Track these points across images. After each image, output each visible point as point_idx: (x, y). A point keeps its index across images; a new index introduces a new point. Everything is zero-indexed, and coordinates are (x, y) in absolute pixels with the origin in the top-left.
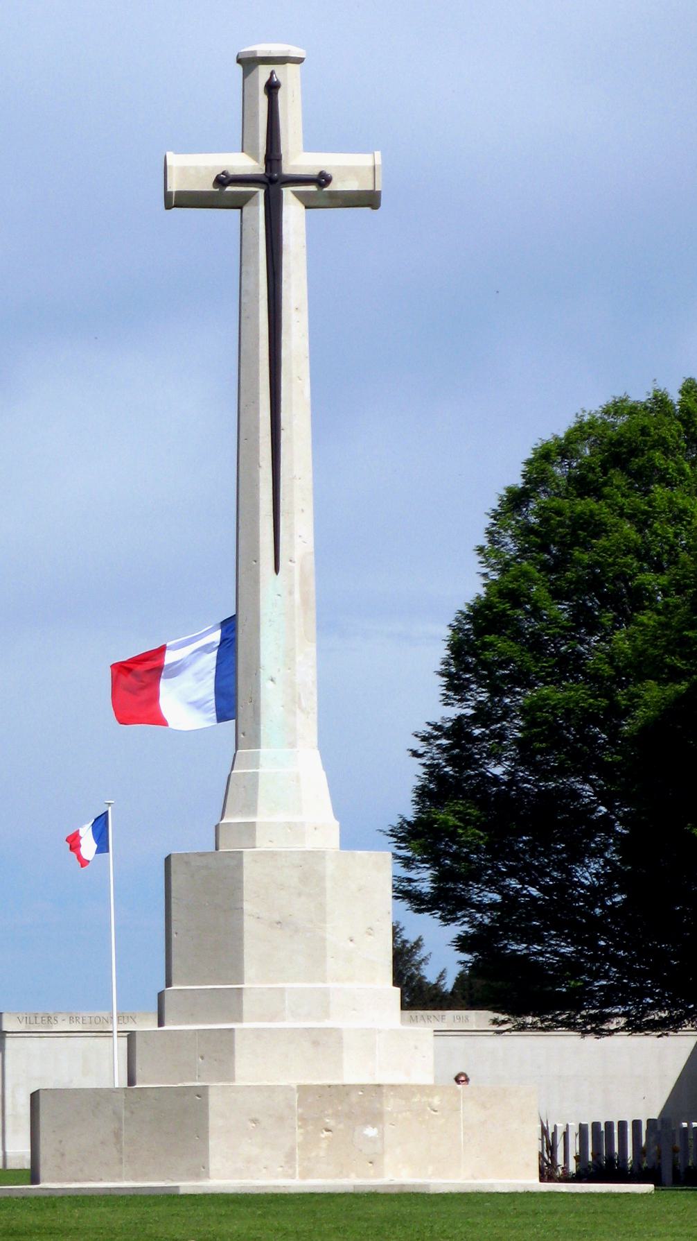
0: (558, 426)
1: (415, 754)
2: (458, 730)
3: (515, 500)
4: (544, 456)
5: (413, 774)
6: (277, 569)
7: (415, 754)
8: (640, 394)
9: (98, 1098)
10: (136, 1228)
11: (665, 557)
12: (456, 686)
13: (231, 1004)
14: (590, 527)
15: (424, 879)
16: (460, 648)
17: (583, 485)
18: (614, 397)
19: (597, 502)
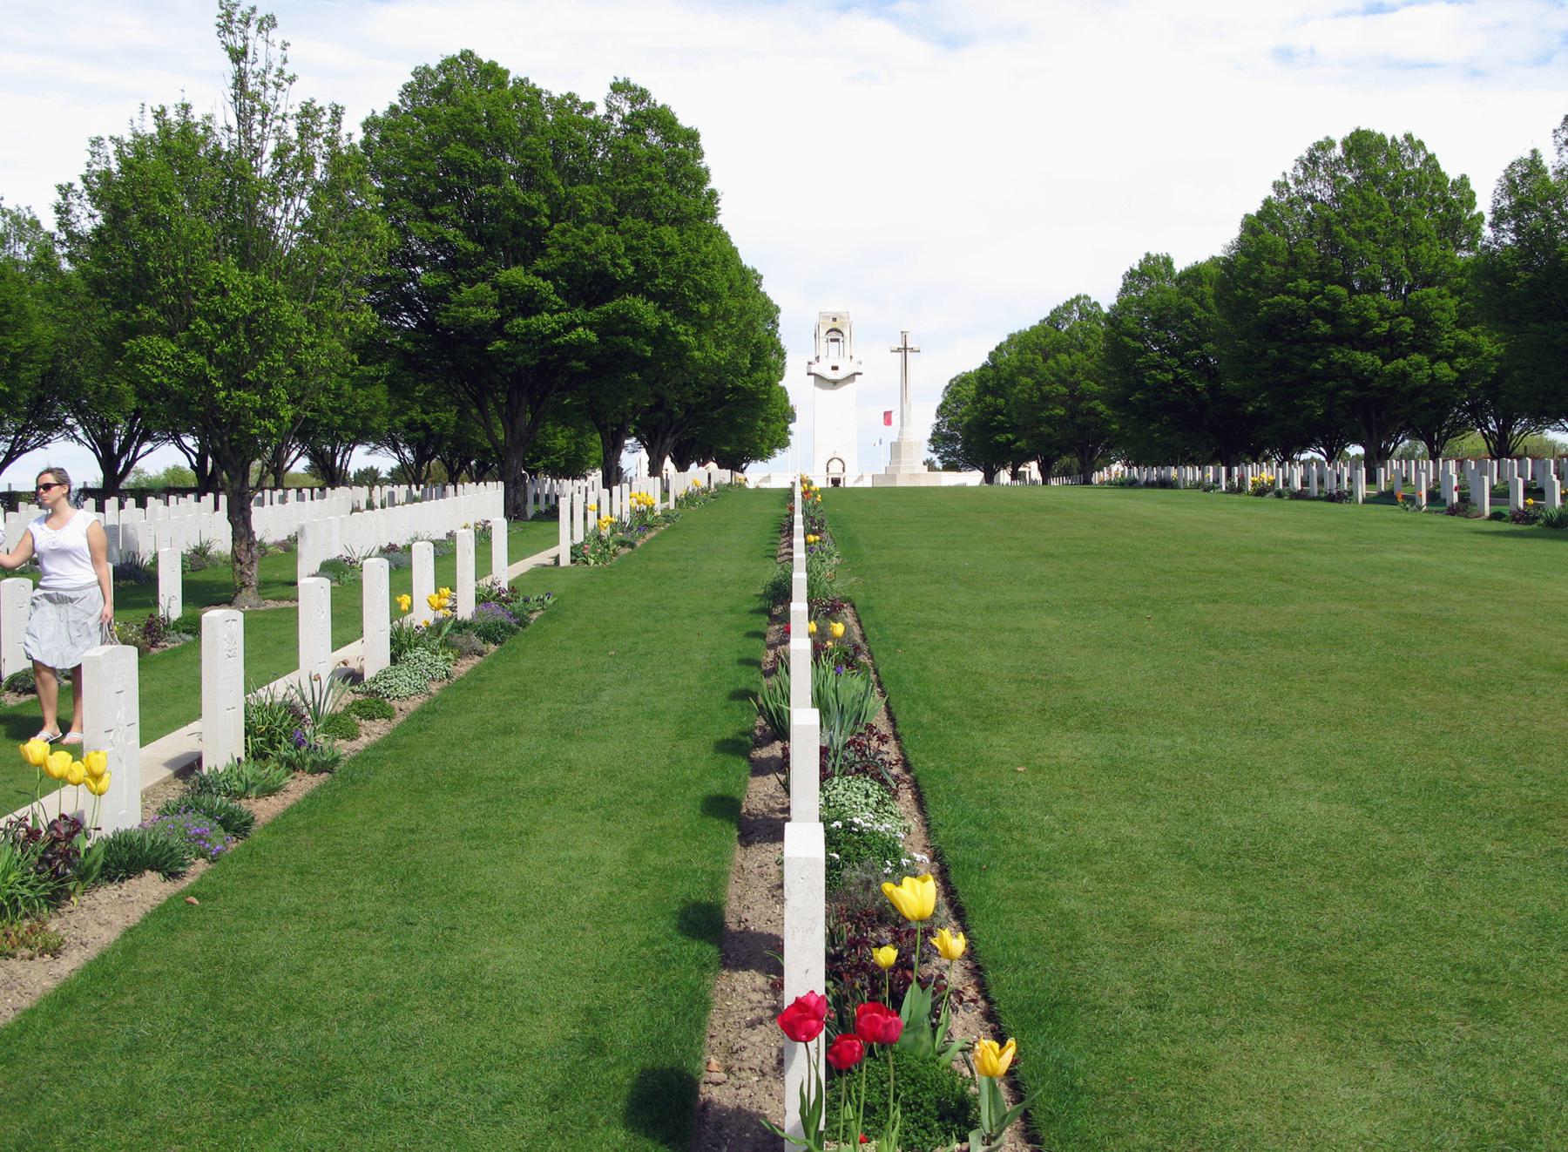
0: (954, 376)
1: (1285, 174)
2: (938, 424)
3: (947, 387)
4: (952, 380)
5: (931, 431)
6: (271, 504)
7: (1285, 174)
8: (967, 371)
9: (881, 476)
10: (475, 952)
11: (617, 788)
12: (938, 417)
13: (900, 463)
14: (958, 392)
15: (932, 448)
16: (938, 411)
17: (958, 385)
18: (616, 78)
19: (1501, 449)
